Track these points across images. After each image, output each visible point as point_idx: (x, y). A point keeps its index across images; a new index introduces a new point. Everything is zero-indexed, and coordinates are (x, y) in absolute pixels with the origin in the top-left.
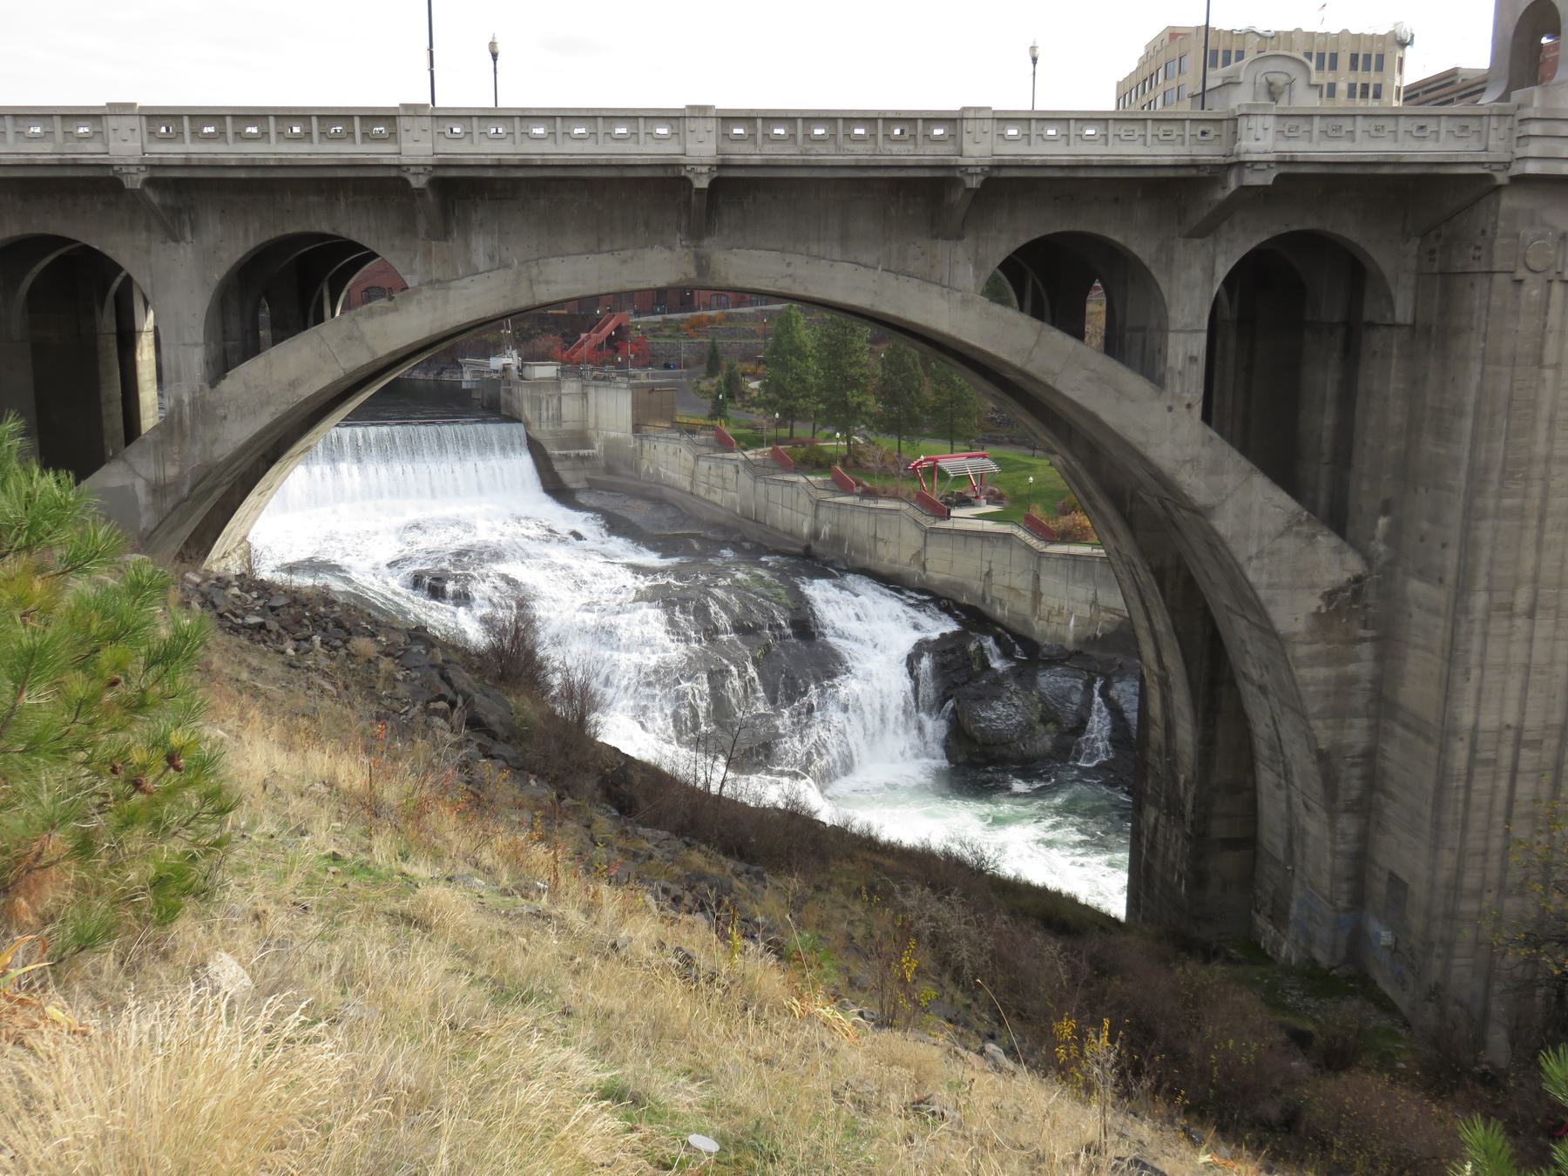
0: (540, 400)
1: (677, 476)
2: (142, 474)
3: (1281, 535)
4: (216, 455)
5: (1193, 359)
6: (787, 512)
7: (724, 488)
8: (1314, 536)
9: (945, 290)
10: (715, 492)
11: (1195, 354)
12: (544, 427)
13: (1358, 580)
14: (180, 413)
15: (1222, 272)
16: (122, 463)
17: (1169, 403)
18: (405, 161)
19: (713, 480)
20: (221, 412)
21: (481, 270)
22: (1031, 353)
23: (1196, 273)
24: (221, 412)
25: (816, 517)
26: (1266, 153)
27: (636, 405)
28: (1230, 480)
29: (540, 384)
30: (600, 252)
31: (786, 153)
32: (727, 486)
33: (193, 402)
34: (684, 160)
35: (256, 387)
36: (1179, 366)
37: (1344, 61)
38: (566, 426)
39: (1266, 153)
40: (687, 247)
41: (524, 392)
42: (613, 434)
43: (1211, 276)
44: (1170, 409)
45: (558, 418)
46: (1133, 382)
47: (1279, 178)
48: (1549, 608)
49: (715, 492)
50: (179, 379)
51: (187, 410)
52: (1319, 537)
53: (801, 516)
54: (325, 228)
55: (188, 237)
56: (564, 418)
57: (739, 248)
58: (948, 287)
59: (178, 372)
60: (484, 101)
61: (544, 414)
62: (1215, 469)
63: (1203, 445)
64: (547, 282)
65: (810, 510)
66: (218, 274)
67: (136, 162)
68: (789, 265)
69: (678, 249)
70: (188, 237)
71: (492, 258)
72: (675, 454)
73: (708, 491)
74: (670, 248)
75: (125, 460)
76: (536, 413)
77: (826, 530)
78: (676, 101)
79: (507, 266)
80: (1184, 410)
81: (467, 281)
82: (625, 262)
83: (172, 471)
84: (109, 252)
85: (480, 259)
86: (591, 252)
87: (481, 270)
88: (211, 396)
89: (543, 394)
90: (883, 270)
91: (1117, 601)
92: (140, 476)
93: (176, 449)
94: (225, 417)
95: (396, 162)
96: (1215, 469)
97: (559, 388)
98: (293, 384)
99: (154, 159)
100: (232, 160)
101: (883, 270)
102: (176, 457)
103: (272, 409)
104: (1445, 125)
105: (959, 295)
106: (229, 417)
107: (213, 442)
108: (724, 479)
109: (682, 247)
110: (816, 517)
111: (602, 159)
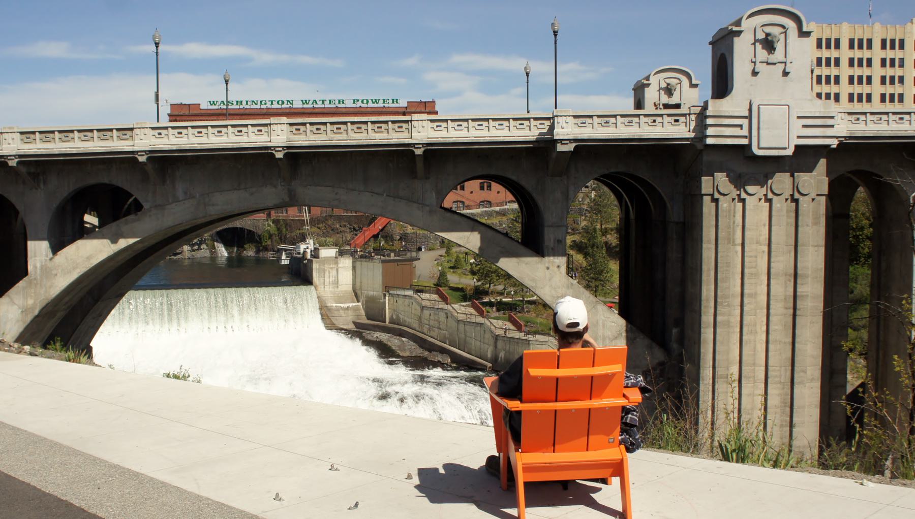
0: (324, 271)
1: (410, 320)
2: (17, 303)
3: (616, 338)
4: (51, 294)
6: (478, 343)
7: (439, 328)
8: (635, 339)
9: (420, 205)
10: (434, 331)
11: (560, 238)
13: (661, 364)
14: (36, 272)
16: (8, 298)
17: (547, 265)
18: (136, 149)
19: (432, 323)
20: (54, 272)
21: (181, 199)
22: (468, 238)
24: (54, 272)
25: (496, 347)
26: (568, 135)
27: (385, 275)
29: (327, 259)
30: (239, 190)
32: (441, 326)
33: (42, 267)
34: (269, 145)
35: (71, 260)
36: (552, 245)
37: (244, 103)
39: (568, 135)
40: (284, 186)
41: (315, 266)
42: (371, 293)
44: (548, 268)
47: (576, 147)
48: (750, 377)
49: (434, 331)
50: (35, 256)
51: (38, 271)
52: (638, 339)
53: (486, 346)
54: (106, 181)
55: (42, 186)
56: (340, 283)
57: (310, 186)
58: (422, 204)
59: (35, 253)
61: (327, 280)
63: (568, 287)
64: (213, 205)
65: (492, 342)
66: (55, 204)
67: (14, 154)
68: (336, 194)
69: (280, 187)
70: (42, 186)
71: (186, 193)
72: (409, 305)
73: (429, 330)
74: (275, 187)
75: (9, 296)
76: (322, 280)
77: (502, 355)
79: (194, 197)
80: (556, 269)
81: (174, 205)
82: (252, 194)
83: (30, 302)
84: (6, 195)
85: (180, 194)
86: (236, 189)
87: (181, 199)
88: (50, 264)
89: (327, 267)
90: (387, 196)
92: (15, 304)
93: (33, 291)
94: (56, 275)
95: (131, 150)
97: (337, 263)
98: (89, 258)
99: (22, 152)
100: (57, 152)
101: (387, 196)
102: (33, 295)
103: (78, 270)
104: (667, 119)
105: (428, 208)
106: (58, 275)
107: (50, 287)
108: (439, 322)
109: (281, 185)
110: (496, 347)
111: (230, 146)
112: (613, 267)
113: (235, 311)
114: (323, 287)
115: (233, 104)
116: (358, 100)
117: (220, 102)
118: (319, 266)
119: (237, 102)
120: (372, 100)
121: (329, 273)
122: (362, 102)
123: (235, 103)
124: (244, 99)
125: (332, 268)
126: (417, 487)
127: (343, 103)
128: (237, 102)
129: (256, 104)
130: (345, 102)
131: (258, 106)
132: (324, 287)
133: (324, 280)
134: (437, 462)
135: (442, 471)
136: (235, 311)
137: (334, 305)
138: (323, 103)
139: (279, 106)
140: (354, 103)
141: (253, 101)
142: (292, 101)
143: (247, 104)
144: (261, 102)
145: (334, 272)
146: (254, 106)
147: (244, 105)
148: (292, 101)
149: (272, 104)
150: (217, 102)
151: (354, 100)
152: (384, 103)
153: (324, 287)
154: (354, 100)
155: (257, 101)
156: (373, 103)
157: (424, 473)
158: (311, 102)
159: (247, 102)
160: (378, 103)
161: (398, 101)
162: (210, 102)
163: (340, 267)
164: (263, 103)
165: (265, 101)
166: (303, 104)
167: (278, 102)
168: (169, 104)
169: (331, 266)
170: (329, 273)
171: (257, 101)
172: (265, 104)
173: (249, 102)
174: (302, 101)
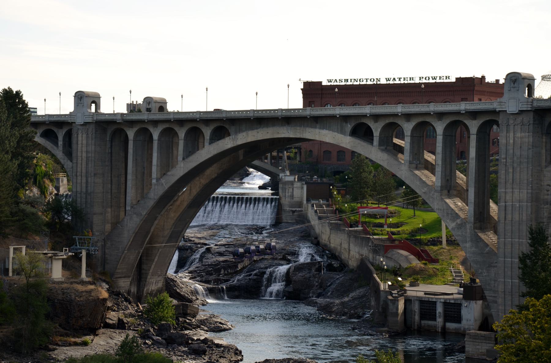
0: (285, 189)
5: (61, 145)
12: (287, 200)
15: (64, 134)
23: (61, 134)
28: (66, 161)
31: (273, 114)
37: (349, 81)
38: (295, 199)
43: (62, 133)
45: (292, 196)
46: (55, 148)
56: (294, 196)
60: (287, 108)
61: (287, 194)
62: (64, 159)
76: (284, 194)
78: (249, 109)
89: (287, 187)
91: (351, 268)
96: (64, 159)
112: (545, 214)
113: (462, 329)
114: (284, 198)
115: (342, 82)
116: (423, 78)
117: (334, 80)
118: (283, 185)
119: (345, 80)
120: (432, 77)
121: (288, 190)
122: (371, 80)
123: (343, 81)
124: (349, 78)
125: (290, 187)
126: (25, 101)
127: (413, 80)
128: (345, 80)
129: (357, 81)
130: (414, 79)
131: (358, 83)
132: (285, 199)
133: (285, 194)
134: (10, 88)
135: (15, 93)
136: (462, 329)
137: (288, 209)
138: (399, 80)
139: (372, 83)
140: (420, 80)
141: (355, 80)
142: (380, 79)
143: (351, 81)
144: (360, 80)
145: (291, 190)
146: (355, 83)
147: (438, 81)
148: (380, 79)
149: (367, 81)
150: (437, 77)
151: (420, 78)
152: (404, 80)
153: (285, 199)
154: (420, 78)
155: (357, 79)
156: (433, 79)
157: (9, 87)
158: (392, 80)
159: (351, 80)
160: (436, 79)
161: (450, 78)
162: (328, 80)
163: (295, 187)
164: (361, 81)
165: (363, 79)
166: (387, 81)
167: (371, 80)
168: (302, 82)
169: (290, 186)
170: (288, 190)
171: (357, 79)
172: (363, 81)
173: (352, 80)
174: (386, 79)
